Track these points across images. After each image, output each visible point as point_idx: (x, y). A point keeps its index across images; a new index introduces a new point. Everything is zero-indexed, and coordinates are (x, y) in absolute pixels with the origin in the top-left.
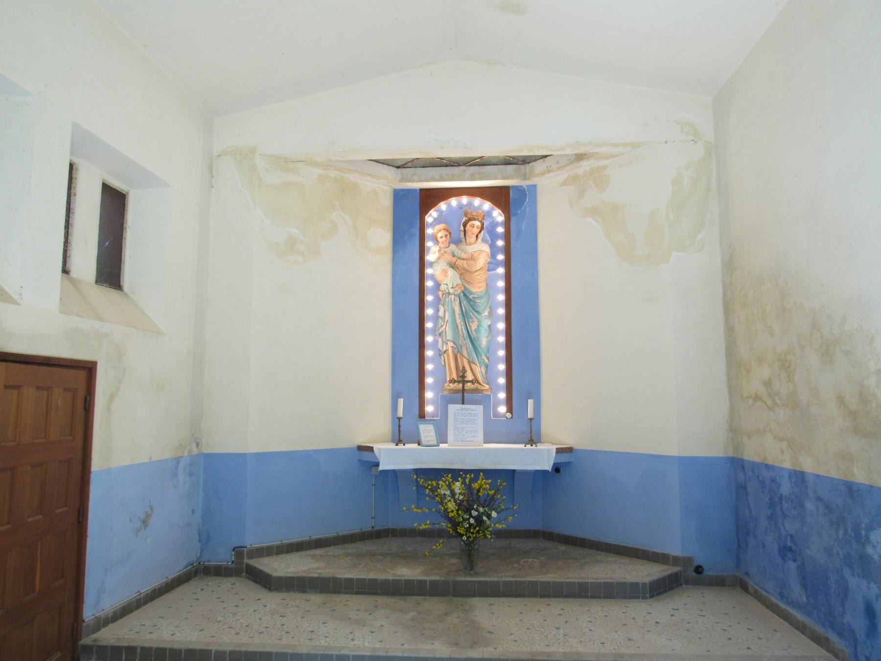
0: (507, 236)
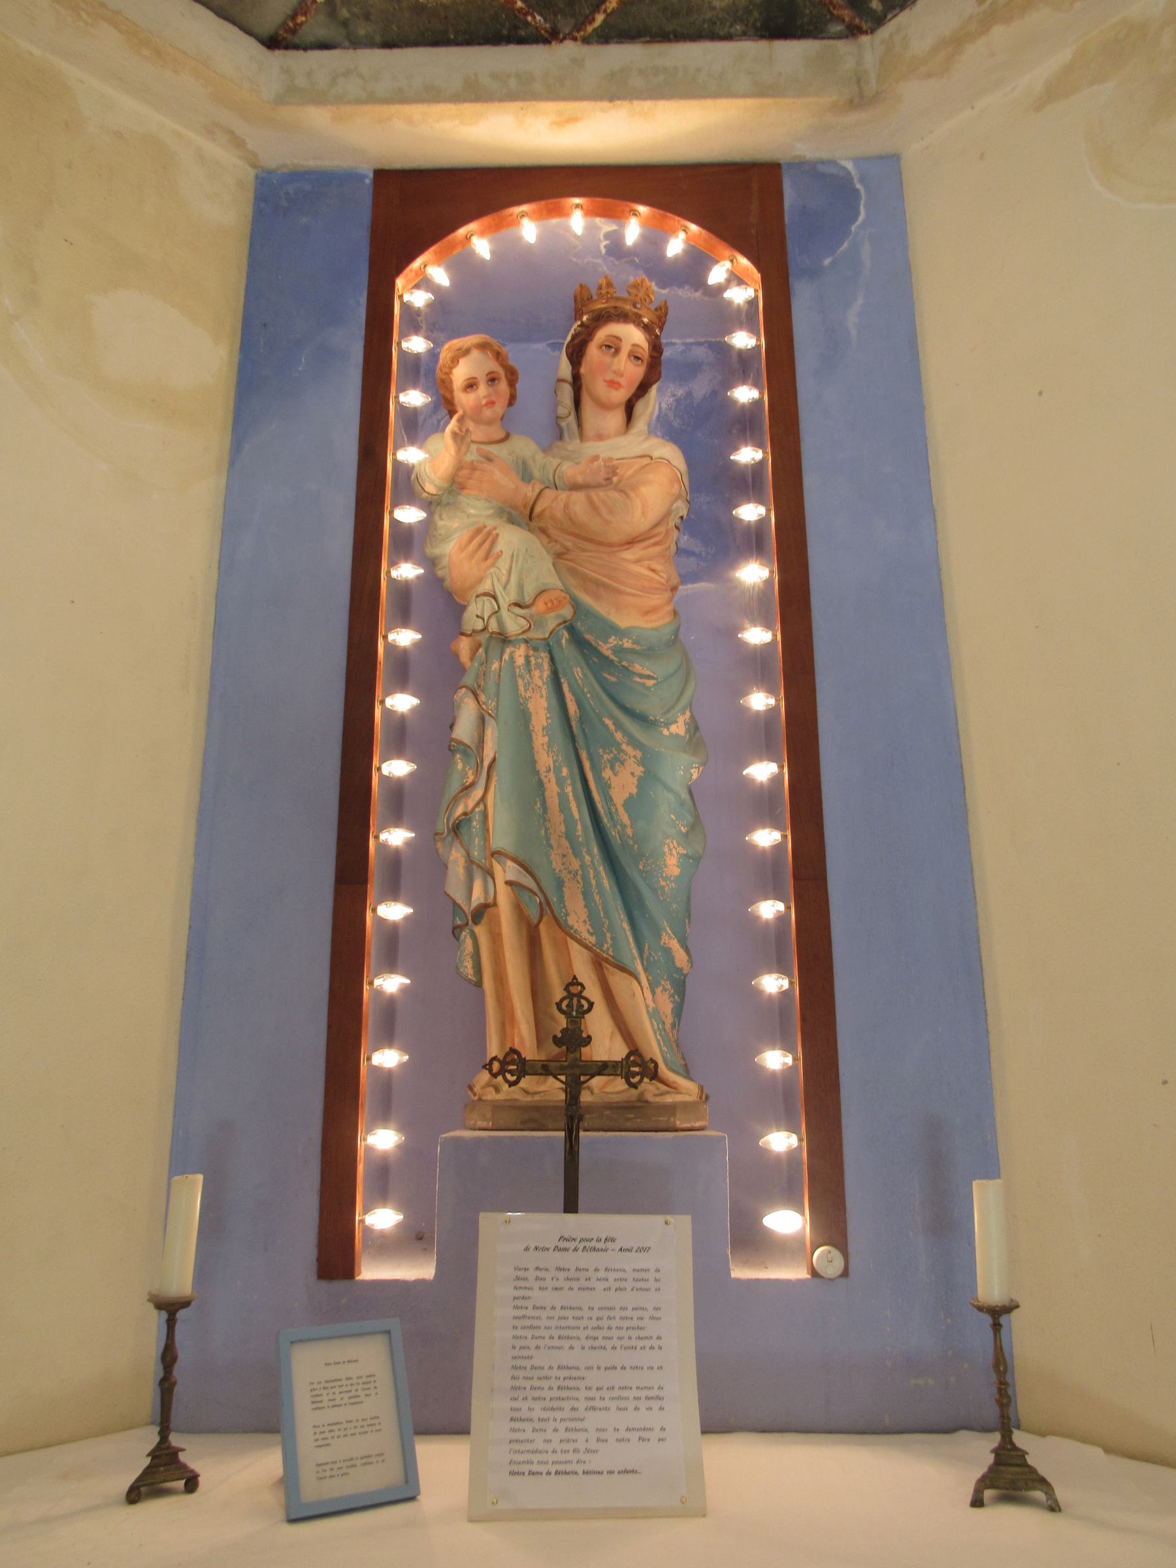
0: (779, 365)
